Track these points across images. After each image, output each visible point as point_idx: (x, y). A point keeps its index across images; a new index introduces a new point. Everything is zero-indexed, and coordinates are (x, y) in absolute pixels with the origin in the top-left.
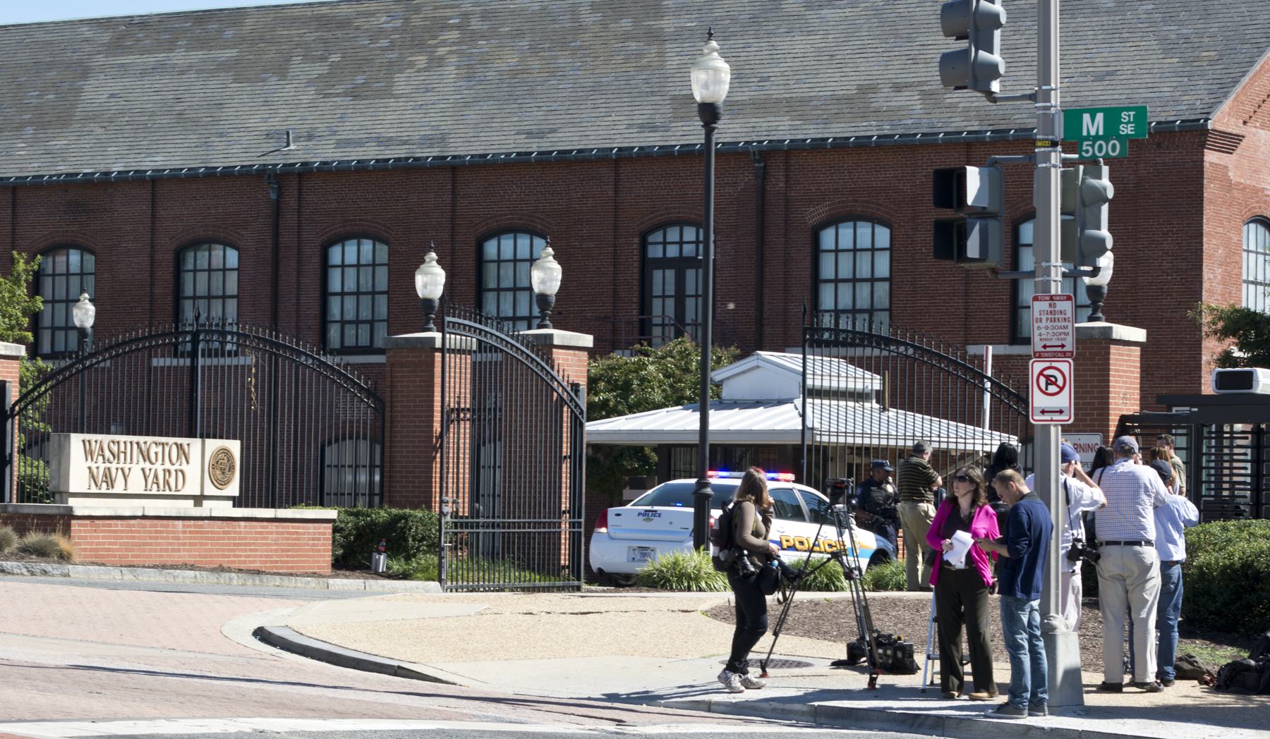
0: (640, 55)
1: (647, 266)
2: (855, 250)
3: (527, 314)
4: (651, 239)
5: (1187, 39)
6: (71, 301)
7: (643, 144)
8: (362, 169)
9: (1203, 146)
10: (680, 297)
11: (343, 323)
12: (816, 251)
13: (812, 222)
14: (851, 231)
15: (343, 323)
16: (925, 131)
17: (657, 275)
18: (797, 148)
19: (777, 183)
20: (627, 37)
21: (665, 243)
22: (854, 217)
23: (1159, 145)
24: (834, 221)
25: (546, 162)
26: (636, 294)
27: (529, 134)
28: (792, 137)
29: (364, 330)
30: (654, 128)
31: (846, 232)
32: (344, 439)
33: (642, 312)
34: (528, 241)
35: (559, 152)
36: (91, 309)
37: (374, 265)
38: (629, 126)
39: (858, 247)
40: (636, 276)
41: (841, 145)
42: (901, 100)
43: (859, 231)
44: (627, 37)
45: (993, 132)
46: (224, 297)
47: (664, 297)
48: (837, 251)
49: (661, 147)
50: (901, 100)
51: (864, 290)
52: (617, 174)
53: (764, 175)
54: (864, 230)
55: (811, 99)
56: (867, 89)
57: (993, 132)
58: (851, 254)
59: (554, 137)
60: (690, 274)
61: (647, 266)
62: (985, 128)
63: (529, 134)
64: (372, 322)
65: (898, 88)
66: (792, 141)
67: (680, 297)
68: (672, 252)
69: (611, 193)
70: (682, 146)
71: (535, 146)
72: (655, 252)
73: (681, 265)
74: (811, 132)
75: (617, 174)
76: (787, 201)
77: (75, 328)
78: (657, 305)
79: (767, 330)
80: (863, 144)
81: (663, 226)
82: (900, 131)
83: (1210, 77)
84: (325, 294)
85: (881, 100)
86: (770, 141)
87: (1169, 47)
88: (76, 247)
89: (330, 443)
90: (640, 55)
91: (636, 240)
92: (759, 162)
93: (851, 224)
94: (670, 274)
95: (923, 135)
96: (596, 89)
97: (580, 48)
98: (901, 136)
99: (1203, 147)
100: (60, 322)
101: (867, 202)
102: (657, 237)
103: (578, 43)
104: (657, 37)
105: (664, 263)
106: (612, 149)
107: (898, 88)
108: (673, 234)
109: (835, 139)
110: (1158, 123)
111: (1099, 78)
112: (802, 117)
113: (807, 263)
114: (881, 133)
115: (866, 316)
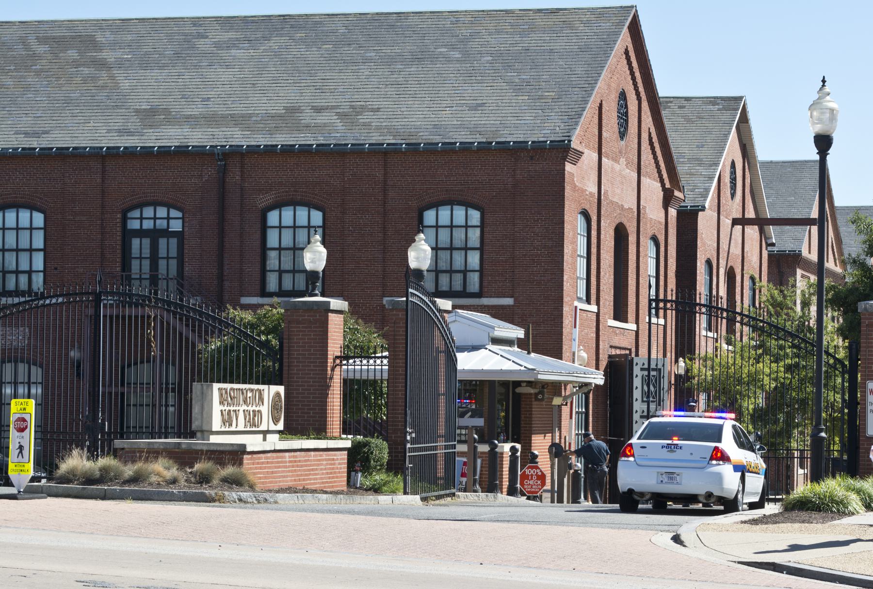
0: (94, 79)
1: (127, 235)
2: (17, 229)
3: (28, 269)
4: (130, 215)
5: (528, 83)
6: (297, 250)
7: (126, 145)
8: (449, 150)
9: (564, 159)
10: (154, 259)
11: (281, 272)
12: (264, 227)
13: (261, 206)
14: (449, 212)
15: (281, 272)
16: (354, 142)
17: (136, 242)
18: (253, 151)
19: (234, 176)
20: (77, 64)
21: (141, 218)
22: (294, 203)
23: (532, 158)
24: (278, 205)
25: (47, 154)
26: (119, 256)
27: (26, 134)
28: (248, 144)
29: (458, 279)
30: (130, 133)
31: (287, 214)
32: (142, 362)
33: (123, 270)
34: (28, 214)
35: (58, 148)
36: (323, 251)
37: (31, 229)
38: (109, 131)
39: (454, 224)
40: (119, 243)
41: (288, 150)
42: (323, 118)
43: (20, 214)
44: (77, 64)
45: (406, 144)
46: (31, 250)
47: (141, 258)
48: (280, 227)
49: (141, 147)
50: (323, 118)
51: (24, 257)
52: (104, 167)
53: (224, 171)
54: (25, 215)
55: (250, 116)
56: (293, 110)
57: (406, 144)
58: (292, 229)
59: (49, 137)
60: (163, 242)
61: (127, 235)
62: (400, 142)
63: (26, 134)
64: (30, 273)
65: (318, 110)
66: (248, 146)
67: (154, 259)
68: (148, 225)
69: (99, 180)
70: (159, 147)
71: (35, 143)
72: (134, 225)
73: (155, 235)
74: (262, 140)
75: (104, 167)
76: (242, 189)
77: (305, 271)
78: (135, 264)
79: (227, 284)
80: (305, 150)
81: (141, 206)
82: (334, 142)
83: (558, 110)
84: (264, 248)
85: (308, 117)
86: (230, 146)
87: (518, 89)
88: (460, 203)
89: (129, 366)
90: (94, 79)
91: (119, 216)
92: (221, 160)
93: (292, 208)
94: (146, 242)
95: (352, 145)
96: (68, 101)
97: (42, 71)
98: (335, 145)
99: (565, 160)
100: (287, 265)
101: (305, 192)
102: (136, 213)
103: (38, 67)
104: (103, 65)
105: (141, 233)
106: (456, 143)
107: (318, 110)
108: (148, 212)
109: (282, 145)
110: (533, 142)
111: (475, 108)
112: (248, 128)
113: (258, 235)
114: (319, 142)
115: (26, 276)
